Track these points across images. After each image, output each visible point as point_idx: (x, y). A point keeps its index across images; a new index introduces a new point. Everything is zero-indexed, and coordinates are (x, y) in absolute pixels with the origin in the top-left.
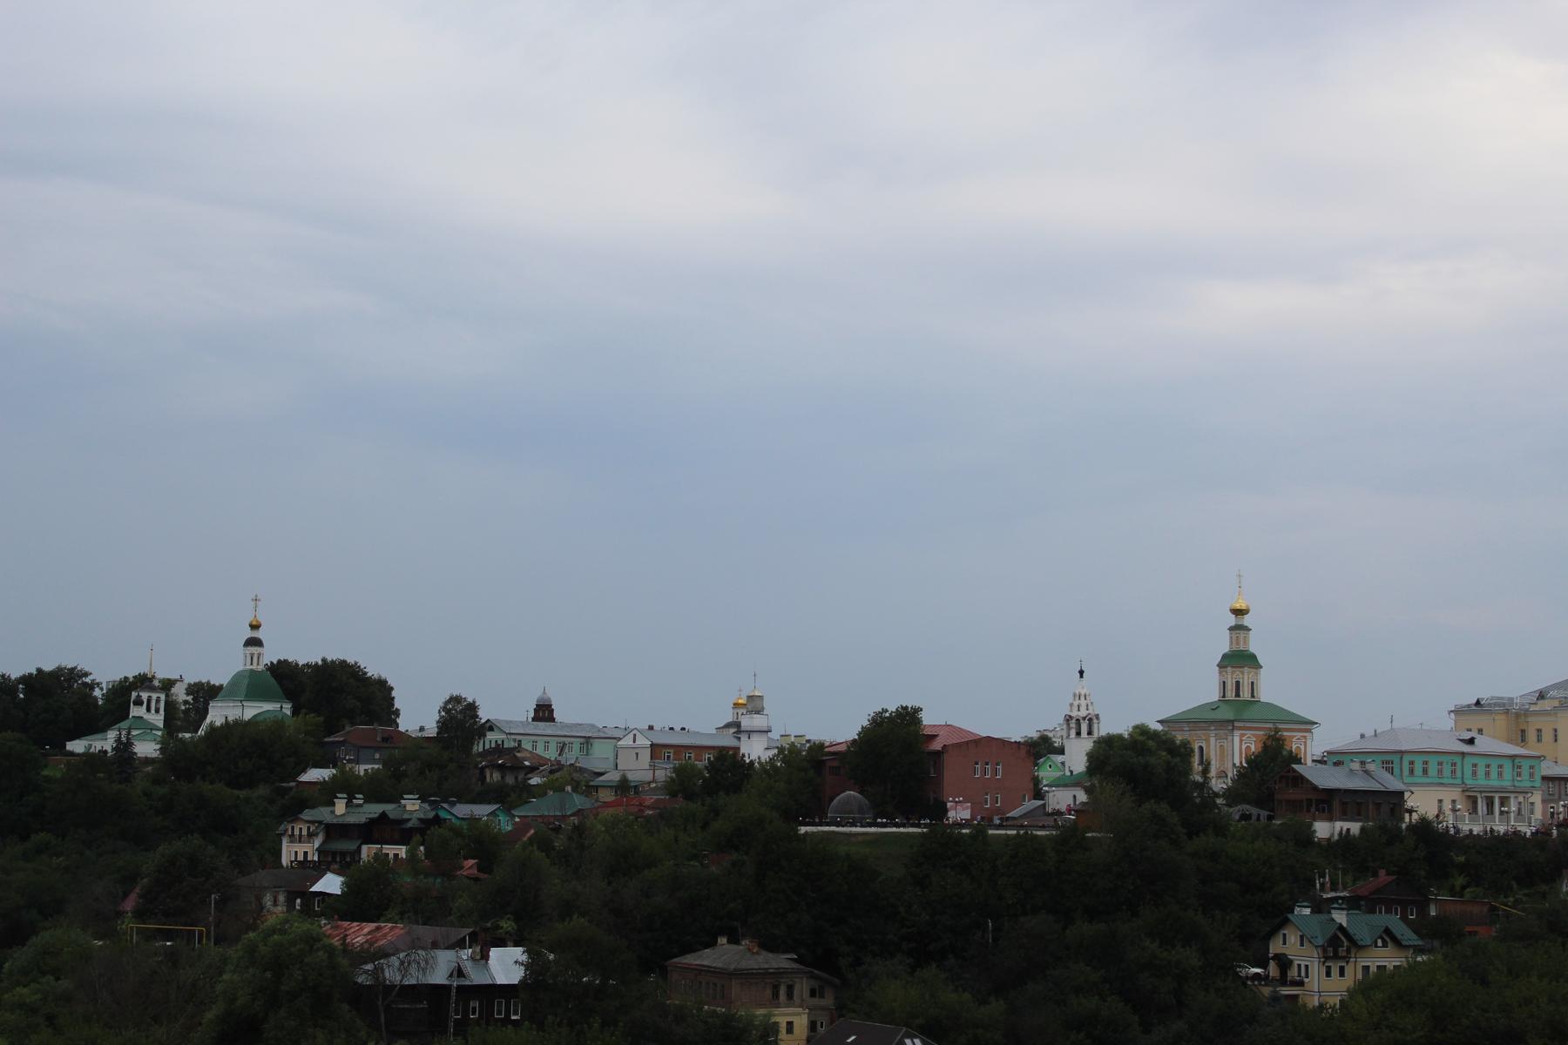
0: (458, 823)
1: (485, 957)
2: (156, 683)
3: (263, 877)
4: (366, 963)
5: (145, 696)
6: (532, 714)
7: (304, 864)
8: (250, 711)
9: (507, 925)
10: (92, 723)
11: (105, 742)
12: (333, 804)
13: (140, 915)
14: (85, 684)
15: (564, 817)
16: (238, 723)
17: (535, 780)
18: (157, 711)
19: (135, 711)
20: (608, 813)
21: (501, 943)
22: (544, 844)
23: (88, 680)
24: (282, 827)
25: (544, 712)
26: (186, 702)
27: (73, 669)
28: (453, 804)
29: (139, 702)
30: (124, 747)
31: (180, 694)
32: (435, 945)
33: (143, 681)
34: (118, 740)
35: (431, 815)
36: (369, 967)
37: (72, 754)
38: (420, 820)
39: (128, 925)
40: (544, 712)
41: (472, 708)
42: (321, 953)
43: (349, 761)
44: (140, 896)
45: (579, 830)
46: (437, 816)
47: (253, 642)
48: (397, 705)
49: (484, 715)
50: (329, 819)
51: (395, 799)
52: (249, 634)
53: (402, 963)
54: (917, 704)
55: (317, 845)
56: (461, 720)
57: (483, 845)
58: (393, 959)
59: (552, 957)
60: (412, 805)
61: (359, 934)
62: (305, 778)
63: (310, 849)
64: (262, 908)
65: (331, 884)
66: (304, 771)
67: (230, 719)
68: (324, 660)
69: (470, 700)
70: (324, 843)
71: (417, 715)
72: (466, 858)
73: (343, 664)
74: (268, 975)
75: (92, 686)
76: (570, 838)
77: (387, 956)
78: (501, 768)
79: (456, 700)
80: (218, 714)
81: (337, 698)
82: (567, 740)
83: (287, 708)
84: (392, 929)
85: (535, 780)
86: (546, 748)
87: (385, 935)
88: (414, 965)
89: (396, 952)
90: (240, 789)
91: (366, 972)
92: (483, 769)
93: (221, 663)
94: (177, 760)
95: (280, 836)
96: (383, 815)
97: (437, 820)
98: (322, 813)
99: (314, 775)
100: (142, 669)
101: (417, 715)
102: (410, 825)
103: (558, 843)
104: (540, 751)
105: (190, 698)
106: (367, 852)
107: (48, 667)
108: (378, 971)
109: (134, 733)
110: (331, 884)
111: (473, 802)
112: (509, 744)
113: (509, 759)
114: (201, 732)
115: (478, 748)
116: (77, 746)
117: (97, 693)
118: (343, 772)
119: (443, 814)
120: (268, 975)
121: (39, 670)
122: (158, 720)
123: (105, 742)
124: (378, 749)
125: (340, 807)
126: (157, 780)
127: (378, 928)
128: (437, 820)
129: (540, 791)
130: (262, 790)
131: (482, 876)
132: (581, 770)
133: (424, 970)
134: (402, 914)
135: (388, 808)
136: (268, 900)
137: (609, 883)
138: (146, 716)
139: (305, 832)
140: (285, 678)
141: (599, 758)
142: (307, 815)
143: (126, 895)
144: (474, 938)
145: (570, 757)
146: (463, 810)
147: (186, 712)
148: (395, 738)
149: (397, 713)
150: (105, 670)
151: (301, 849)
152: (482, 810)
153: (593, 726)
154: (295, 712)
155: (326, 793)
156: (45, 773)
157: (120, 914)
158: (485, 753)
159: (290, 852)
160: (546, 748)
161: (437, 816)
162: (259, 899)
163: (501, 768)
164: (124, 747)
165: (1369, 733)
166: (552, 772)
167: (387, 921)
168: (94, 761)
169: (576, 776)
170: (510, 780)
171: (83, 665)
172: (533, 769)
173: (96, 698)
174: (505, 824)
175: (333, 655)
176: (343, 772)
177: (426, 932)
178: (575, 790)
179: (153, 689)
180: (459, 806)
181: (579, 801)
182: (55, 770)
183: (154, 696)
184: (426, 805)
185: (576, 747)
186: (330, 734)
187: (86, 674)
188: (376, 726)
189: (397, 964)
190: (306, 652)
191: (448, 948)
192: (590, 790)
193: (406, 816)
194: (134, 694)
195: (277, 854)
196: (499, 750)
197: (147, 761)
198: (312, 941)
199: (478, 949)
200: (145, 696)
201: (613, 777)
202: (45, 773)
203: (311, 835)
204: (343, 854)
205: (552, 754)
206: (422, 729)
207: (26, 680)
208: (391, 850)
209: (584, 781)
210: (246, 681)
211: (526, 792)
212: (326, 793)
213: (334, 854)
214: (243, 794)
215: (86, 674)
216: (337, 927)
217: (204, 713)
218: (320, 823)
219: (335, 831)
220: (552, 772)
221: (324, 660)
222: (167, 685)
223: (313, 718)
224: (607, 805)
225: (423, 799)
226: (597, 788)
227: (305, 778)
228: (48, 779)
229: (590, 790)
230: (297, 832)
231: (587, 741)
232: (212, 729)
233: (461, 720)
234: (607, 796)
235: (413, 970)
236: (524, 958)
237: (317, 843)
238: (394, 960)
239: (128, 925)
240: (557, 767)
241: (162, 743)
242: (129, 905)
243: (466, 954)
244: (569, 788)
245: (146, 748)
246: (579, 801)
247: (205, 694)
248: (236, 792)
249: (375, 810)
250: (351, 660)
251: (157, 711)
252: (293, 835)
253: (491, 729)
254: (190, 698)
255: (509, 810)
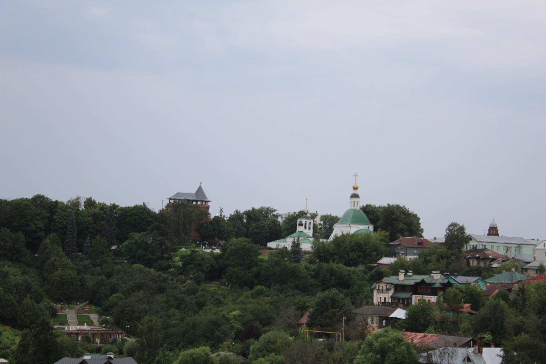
0: (459, 286)
1: (480, 352)
2: (308, 215)
3: (365, 309)
4: (423, 352)
5: (304, 221)
6: (487, 232)
7: (384, 303)
8: (354, 229)
9: (488, 337)
10: (278, 232)
11: (287, 243)
12: (398, 275)
13: (310, 325)
14: (274, 215)
15: (513, 284)
16: (348, 235)
17: (495, 265)
18: (309, 228)
19: (299, 229)
20: (534, 283)
21: (488, 345)
22: (503, 296)
23: (275, 213)
24: (373, 286)
25: (493, 231)
26: (320, 224)
27: (268, 208)
28: (456, 276)
29: (301, 224)
30: (296, 245)
31: (318, 221)
32: (455, 345)
33: (302, 214)
34: (294, 242)
35: (446, 281)
36: (425, 354)
37: (270, 249)
38: (441, 284)
39: (304, 330)
40: (493, 231)
41: (462, 229)
42: (403, 347)
43: (402, 254)
44: (309, 317)
45: (522, 291)
46: (449, 282)
47: (355, 196)
48: (422, 226)
49: (468, 232)
50: (396, 282)
51: (428, 272)
52: (353, 192)
53: (441, 353)
54: (235, 210)
55: (390, 295)
56: (457, 237)
57: (474, 298)
58: (436, 351)
59: (515, 353)
60: (437, 278)
61: (416, 338)
62: (382, 261)
63: (388, 296)
64: (367, 324)
65: (400, 313)
66: (381, 258)
67: (345, 233)
68: (389, 205)
69: (461, 225)
70: (394, 293)
71: (434, 231)
72: (465, 303)
73: (398, 207)
74: (378, 356)
75: (277, 216)
76: (518, 295)
77: (433, 349)
78: (478, 259)
79: (454, 225)
80: (338, 231)
81: (394, 223)
82: (509, 245)
83: (371, 228)
84: (432, 336)
85: (495, 265)
86: (498, 249)
87: (429, 339)
88: (447, 355)
89: (439, 347)
90: (351, 266)
91: (424, 357)
92: (468, 259)
93: (338, 206)
94: (321, 254)
95: (372, 290)
96: (423, 281)
97: (449, 284)
98: (392, 279)
99: (385, 260)
100: (302, 208)
101: (434, 231)
102: (436, 286)
103: (512, 296)
104: (495, 250)
105: (322, 222)
106: (415, 299)
107: (257, 207)
108: (429, 357)
109: (300, 239)
110: (400, 313)
111: (464, 275)
112: (480, 247)
113: (480, 254)
114: (331, 238)
115: (464, 249)
116: (272, 245)
117: (280, 219)
118: (400, 259)
119: (452, 281)
120: (378, 356)
121: (253, 209)
122: (310, 233)
123: (287, 243)
124: (416, 248)
125: (401, 276)
126: (311, 262)
127: (425, 336)
128: (449, 284)
129: (499, 271)
130: (361, 267)
131: (473, 312)
132: (518, 260)
133: (452, 359)
134: (435, 329)
135: (425, 278)
136: (369, 321)
137: (540, 318)
138: (305, 231)
139: (385, 288)
140: (370, 213)
141: (526, 254)
142: (385, 280)
143: (302, 315)
144: (475, 343)
145: (512, 254)
146: (461, 279)
147: (320, 229)
148: (422, 243)
149: (422, 231)
150: (283, 209)
151: (383, 296)
152: (471, 279)
153: (522, 238)
154: (375, 230)
155: (394, 270)
156: (260, 257)
157: (300, 325)
158: (468, 252)
159: (377, 298)
160: (498, 249)
161: (449, 282)
162: (365, 320)
163: (478, 259)
164: (296, 245)
165: (536, 238)
166: (503, 261)
167: (429, 332)
168: (283, 252)
169: (516, 263)
170: (482, 264)
171: (273, 206)
172: (493, 260)
173: (279, 222)
174: (482, 287)
175: (393, 203)
176: (400, 259)
177: (451, 339)
178: (516, 270)
179: (307, 218)
180: (459, 277)
181: (519, 276)
182: (264, 256)
183: (308, 221)
184: (443, 276)
185: (513, 249)
186: (392, 241)
187: (274, 211)
188: (415, 237)
189: (438, 353)
190: (380, 201)
191: (460, 347)
192: (524, 270)
193: (434, 282)
194: (299, 221)
195: (372, 298)
196: (475, 249)
197: (306, 252)
198: (399, 341)
199: (477, 348)
200: (304, 221)
201: (535, 264)
202: (260, 257)
203: (387, 290)
204: (403, 299)
205: (502, 252)
206: (435, 239)
207: (248, 213)
208: (427, 298)
209: (522, 267)
210: (352, 215)
211: (491, 272)
212: (394, 270)
213: (399, 299)
214: (352, 269)
215: (274, 211)
216: (405, 335)
217: (331, 230)
218: (392, 284)
219: (399, 288)
220: (503, 261)
221: (389, 205)
222: (314, 216)
223: (385, 233)
224: (533, 278)
225: (442, 273)
226: (527, 269)
227: (382, 261)
228: (261, 261)
229: (524, 270)
230: (381, 288)
231: (519, 246)
232: (336, 238)
233: (457, 237)
234: (533, 274)
235: (446, 357)
236: (502, 353)
237: (391, 293)
238: (437, 352)
239: (304, 330)
240: (505, 260)
241: (313, 243)
242: (304, 320)
243: (471, 350)
244: (513, 270)
245: (306, 246)
246: (519, 276)
247: (330, 221)
248: (349, 268)
249: (418, 278)
250: (401, 205)
251: (309, 228)
252: (379, 290)
253: (471, 239)
254: (322, 222)
255: (484, 279)
